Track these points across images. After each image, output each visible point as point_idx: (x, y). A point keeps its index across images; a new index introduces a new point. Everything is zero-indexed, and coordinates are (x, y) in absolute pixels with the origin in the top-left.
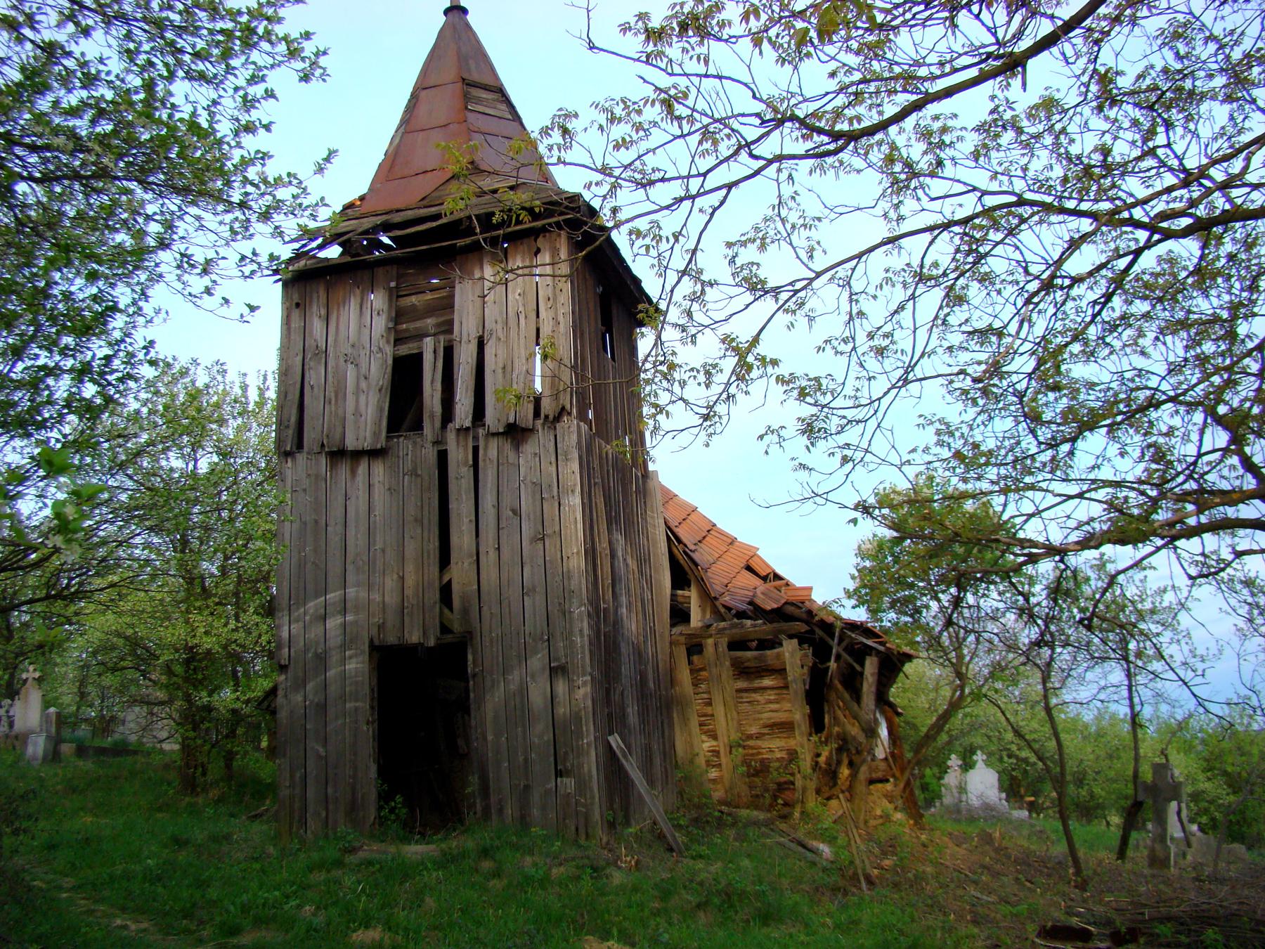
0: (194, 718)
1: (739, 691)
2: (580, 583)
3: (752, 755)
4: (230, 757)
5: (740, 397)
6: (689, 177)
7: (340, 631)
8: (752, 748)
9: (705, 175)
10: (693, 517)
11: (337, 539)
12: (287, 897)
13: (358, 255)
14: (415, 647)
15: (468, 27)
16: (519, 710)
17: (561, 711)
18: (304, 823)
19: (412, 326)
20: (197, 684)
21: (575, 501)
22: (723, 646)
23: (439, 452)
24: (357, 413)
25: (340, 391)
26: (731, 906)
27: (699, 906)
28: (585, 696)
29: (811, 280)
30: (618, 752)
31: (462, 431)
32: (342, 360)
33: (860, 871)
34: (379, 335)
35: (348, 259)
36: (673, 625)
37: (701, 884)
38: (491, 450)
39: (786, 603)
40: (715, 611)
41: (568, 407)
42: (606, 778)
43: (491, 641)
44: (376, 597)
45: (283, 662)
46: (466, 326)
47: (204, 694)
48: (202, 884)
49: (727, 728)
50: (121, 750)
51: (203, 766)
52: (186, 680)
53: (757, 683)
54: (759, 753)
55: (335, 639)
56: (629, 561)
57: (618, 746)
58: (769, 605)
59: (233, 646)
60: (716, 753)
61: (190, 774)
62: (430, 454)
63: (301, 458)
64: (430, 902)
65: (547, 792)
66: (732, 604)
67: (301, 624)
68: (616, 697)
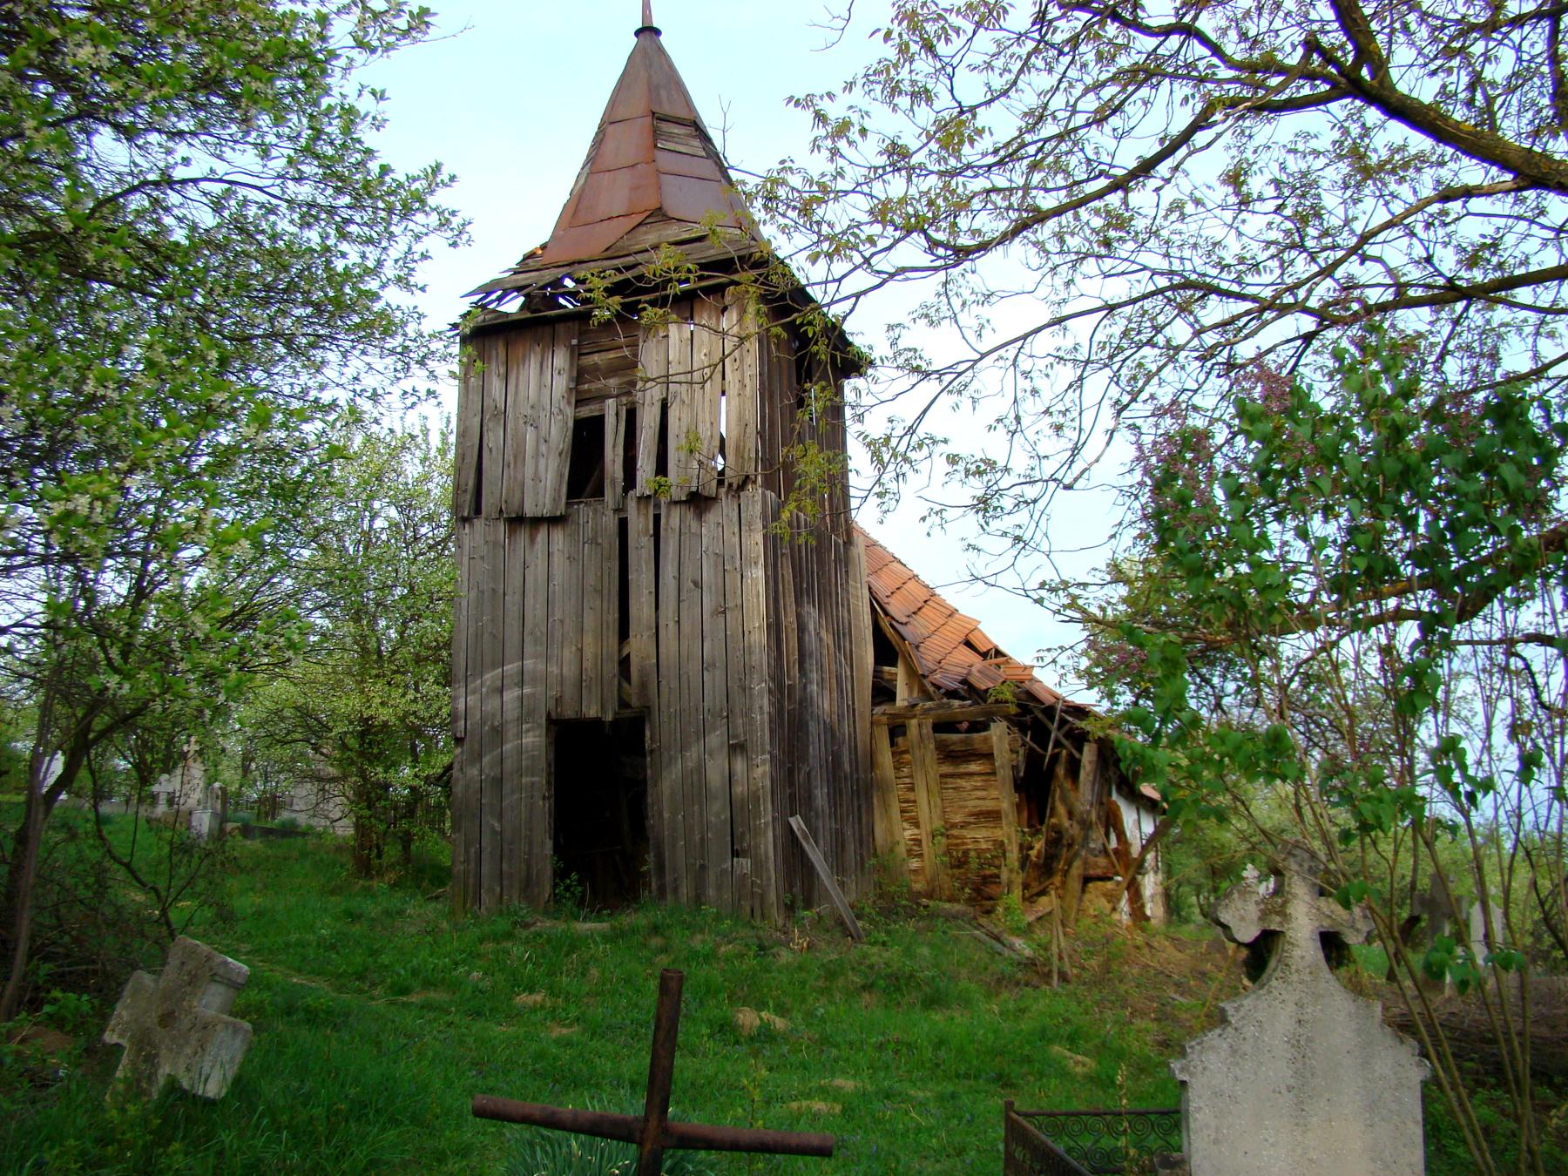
0: (370, 796)
2: (761, 658)
4: (407, 839)
5: (910, 475)
6: (826, 282)
7: (517, 704)
8: (957, 837)
9: (840, 280)
10: (911, 585)
12: (456, 964)
14: (597, 722)
15: (661, 50)
17: (739, 789)
18: (478, 899)
19: (593, 386)
20: (373, 759)
21: (757, 574)
22: (927, 729)
24: (536, 478)
25: (519, 455)
26: (898, 989)
27: (864, 987)
28: (764, 775)
29: (976, 362)
30: (798, 834)
32: (521, 421)
33: (1055, 969)
35: (529, 315)
36: (874, 704)
37: (871, 967)
38: (673, 519)
42: (785, 861)
44: (554, 669)
47: (380, 769)
48: (374, 953)
49: (931, 815)
50: (290, 831)
51: (378, 846)
52: (361, 754)
53: (963, 769)
55: (511, 712)
56: (824, 634)
57: (800, 827)
59: (412, 718)
61: (364, 858)
62: (610, 521)
63: (479, 524)
64: (594, 972)
65: (723, 871)
67: (478, 696)
68: (800, 777)
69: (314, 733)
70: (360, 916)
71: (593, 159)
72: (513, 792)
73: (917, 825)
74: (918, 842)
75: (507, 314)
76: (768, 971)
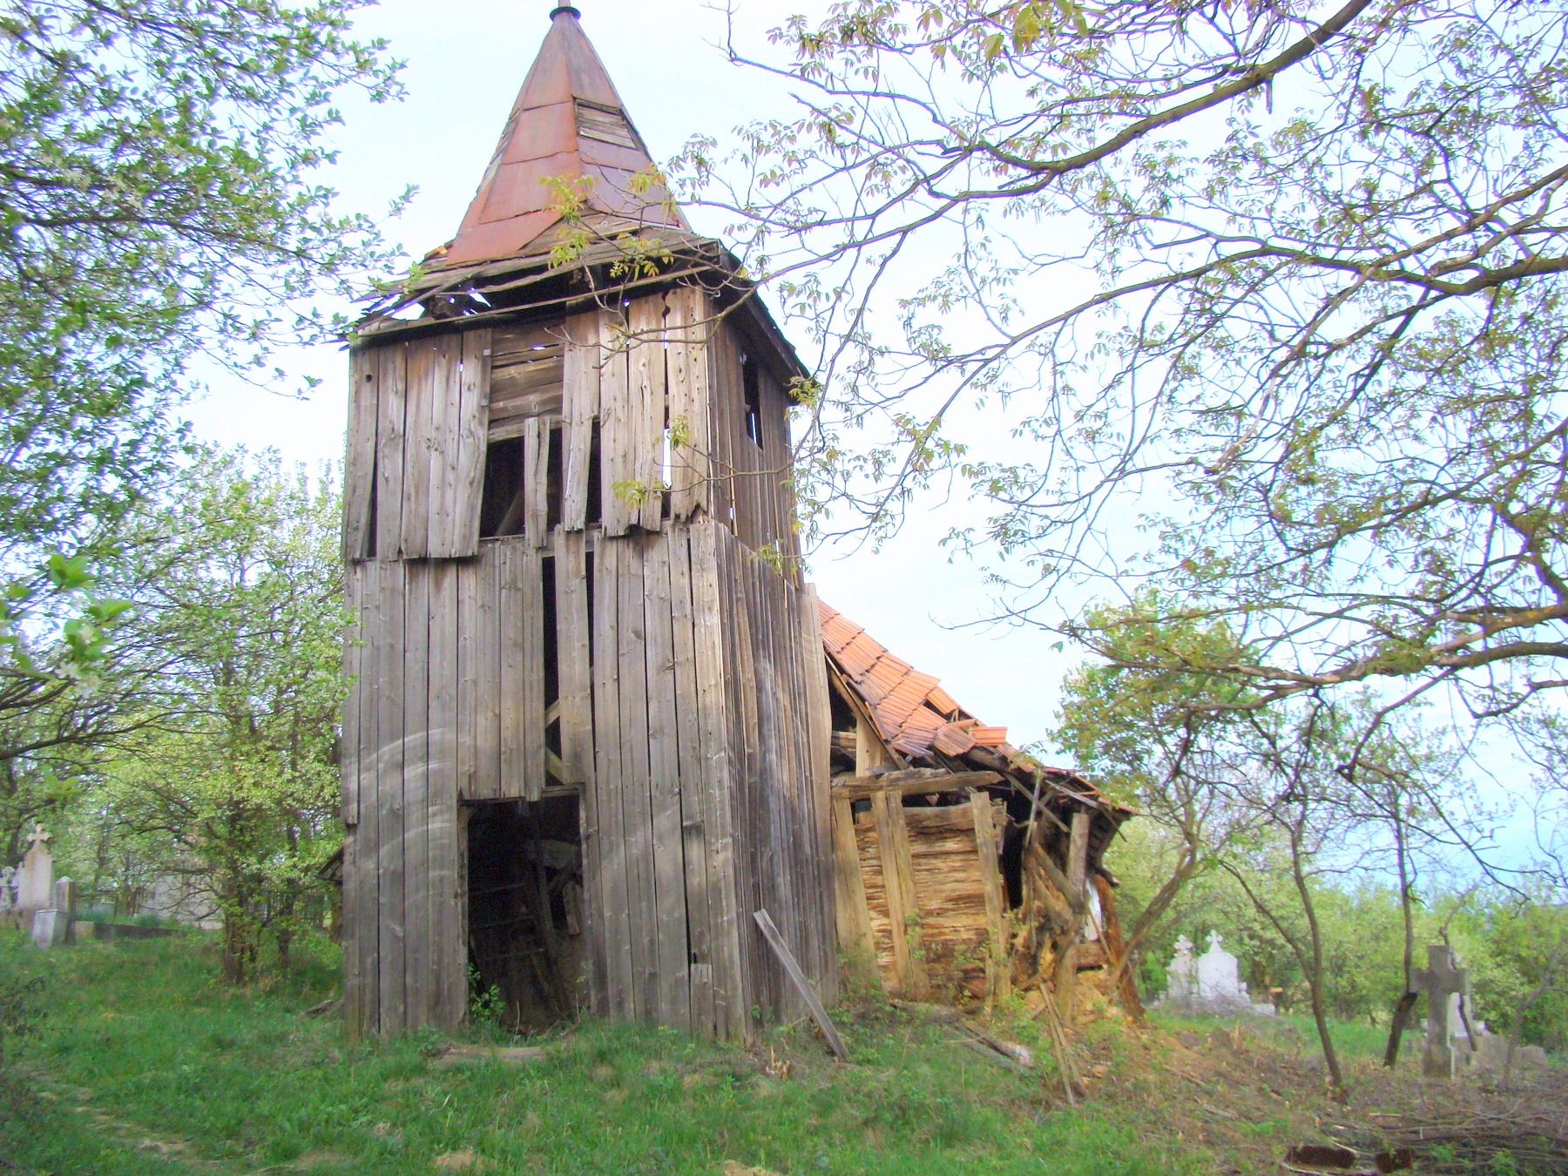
0: (241, 890)
1: (915, 856)
2: (718, 722)
3: (933, 935)
4: (284, 938)
6: (854, 219)
7: (421, 782)
8: (932, 926)
9: (873, 217)
10: (858, 640)
11: (418, 667)
12: (356, 1111)
13: (444, 316)
15: (580, 32)
16: (643, 881)
17: (696, 881)
18: (377, 1020)
19: (510, 404)
20: (244, 848)
21: (712, 621)
22: (896, 801)
23: (544, 560)
24: (442, 512)
26: (907, 1123)
27: (866, 1123)
29: (1006, 347)
30: (766, 932)
31: (573, 534)
32: (424, 446)
34: (469, 416)
35: (431, 321)
36: (834, 775)
37: (869, 1095)
38: (609, 558)
39: (974, 747)
40: (887, 758)
41: (704, 504)
42: (752, 963)
43: (609, 794)
44: (466, 739)
45: (350, 821)
46: (577, 406)
47: (253, 859)
48: (250, 1096)
50: (150, 929)
52: (231, 842)
53: (939, 847)
54: (941, 933)
55: (415, 791)
56: (780, 695)
57: (767, 924)
58: (953, 750)
59: (289, 801)
60: (888, 933)
62: (534, 564)
63: (373, 567)
64: (533, 1118)
65: (678, 981)
66: (907, 748)
67: (373, 774)
68: (763, 864)
69: (176, 818)
70: (231, 1044)
71: (503, 150)
72: (417, 891)
73: (886, 914)
74: (888, 933)
75: (406, 322)
76: (747, 1108)
